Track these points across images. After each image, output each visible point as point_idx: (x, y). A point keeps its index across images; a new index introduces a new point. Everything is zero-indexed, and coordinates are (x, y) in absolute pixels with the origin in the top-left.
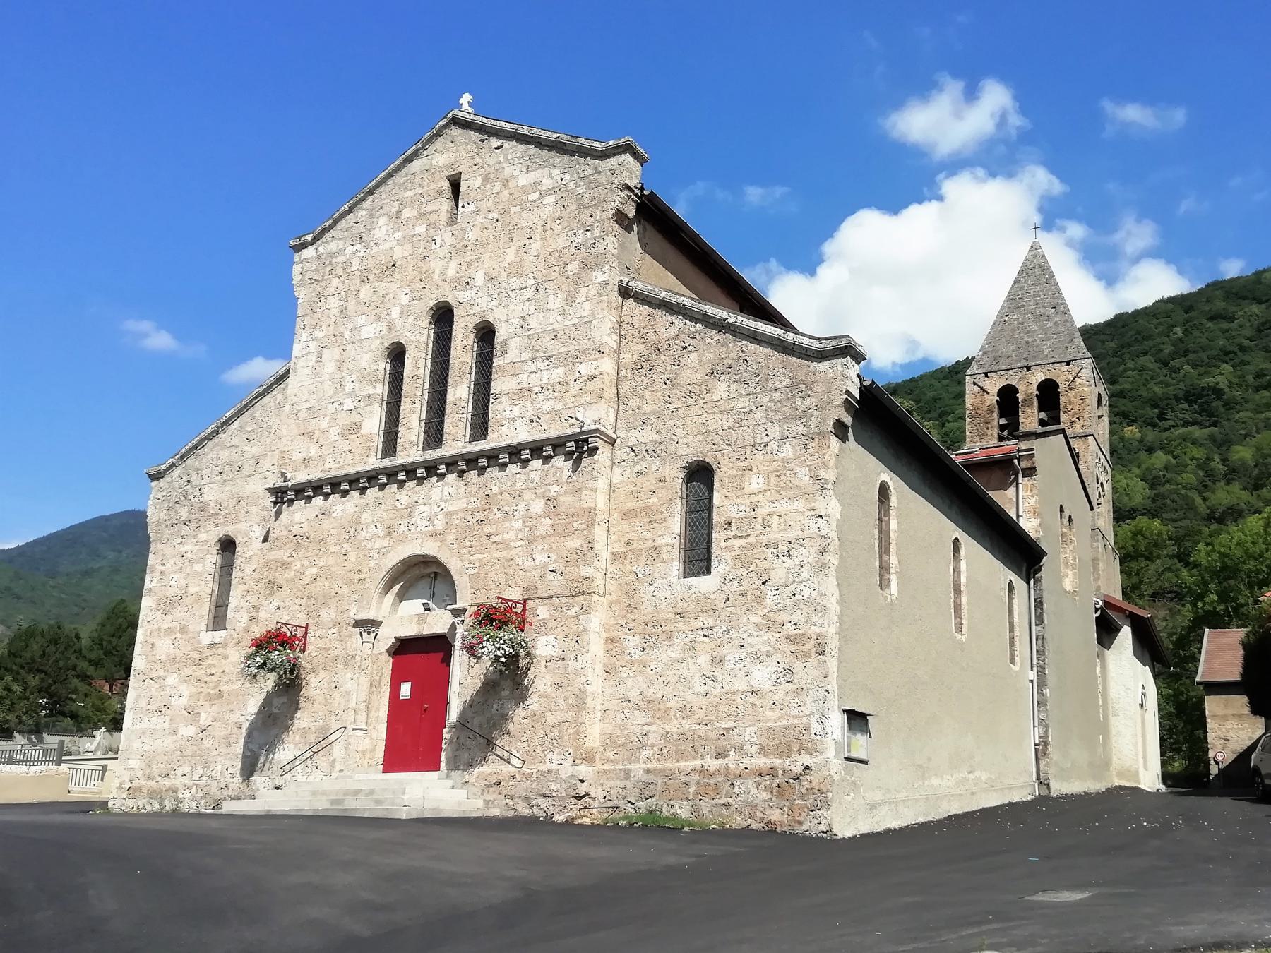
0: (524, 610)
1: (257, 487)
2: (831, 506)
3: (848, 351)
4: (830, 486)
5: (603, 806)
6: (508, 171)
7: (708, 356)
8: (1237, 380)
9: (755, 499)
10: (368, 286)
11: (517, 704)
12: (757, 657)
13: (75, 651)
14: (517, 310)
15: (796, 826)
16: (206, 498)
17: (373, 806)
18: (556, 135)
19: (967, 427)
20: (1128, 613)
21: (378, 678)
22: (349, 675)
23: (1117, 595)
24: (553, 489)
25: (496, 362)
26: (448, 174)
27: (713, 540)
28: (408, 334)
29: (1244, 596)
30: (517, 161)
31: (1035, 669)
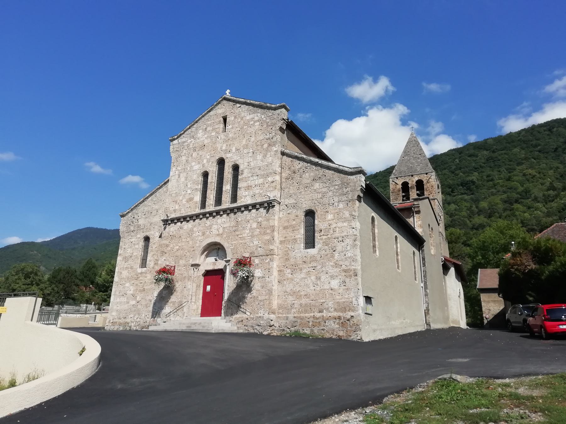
0: (250, 260)
1: (158, 219)
2: (357, 224)
3: (360, 172)
4: (356, 218)
5: (279, 329)
6: (243, 114)
7: (312, 174)
8: (480, 178)
9: (330, 222)
10: (196, 152)
11: (248, 293)
12: (332, 277)
13: (74, 276)
14: (247, 160)
15: (349, 337)
16: (140, 223)
17: (201, 328)
18: (259, 103)
19: (391, 196)
20: (453, 262)
21: (199, 284)
22: (189, 283)
23: (448, 256)
24: (260, 219)
25: (240, 177)
26: (222, 116)
27: (316, 236)
28: (210, 168)
29: (491, 256)
30: (246, 111)
31: (423, 282)
